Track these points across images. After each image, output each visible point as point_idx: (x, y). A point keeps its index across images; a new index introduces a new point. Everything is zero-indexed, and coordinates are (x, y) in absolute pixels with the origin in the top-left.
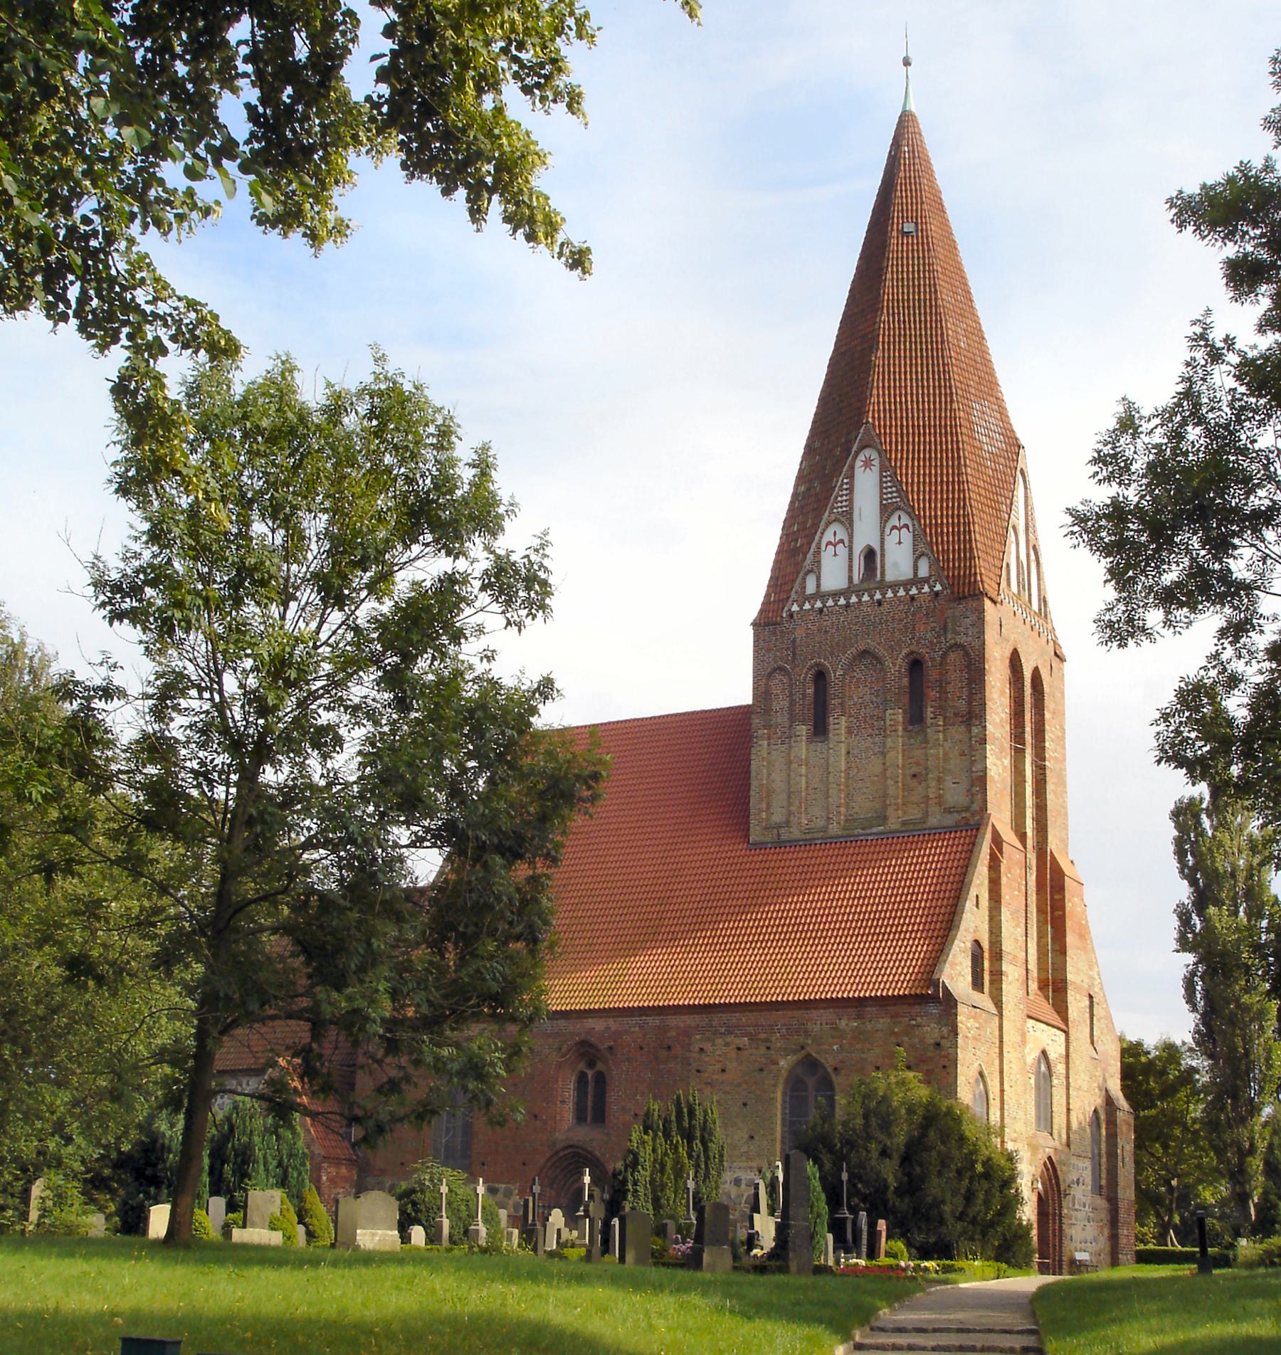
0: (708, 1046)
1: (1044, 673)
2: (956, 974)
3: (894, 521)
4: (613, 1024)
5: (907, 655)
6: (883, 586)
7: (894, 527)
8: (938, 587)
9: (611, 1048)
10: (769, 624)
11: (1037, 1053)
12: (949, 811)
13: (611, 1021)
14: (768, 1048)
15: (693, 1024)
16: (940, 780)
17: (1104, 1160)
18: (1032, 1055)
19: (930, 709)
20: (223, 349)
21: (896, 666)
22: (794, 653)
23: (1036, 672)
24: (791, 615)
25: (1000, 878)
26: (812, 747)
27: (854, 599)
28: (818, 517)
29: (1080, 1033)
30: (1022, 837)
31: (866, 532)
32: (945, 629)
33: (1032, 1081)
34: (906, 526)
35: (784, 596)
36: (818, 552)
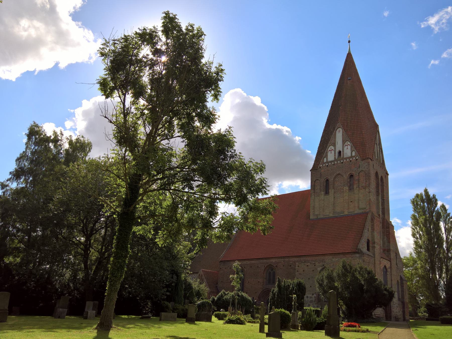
1: (384, 177)
3: (346, 144)
4: (277, 260)
6: (343, 159)
8: (357, 158)
12: (360, 209)
16: (358, 202)
17: (400, 292)
18: (382, 267)
20: (147, 37)
21: (346, 177)
23: (382, 177)
27: (336, 162)
29: (394, 262)
31: (339, 146)
36: (327, 153)
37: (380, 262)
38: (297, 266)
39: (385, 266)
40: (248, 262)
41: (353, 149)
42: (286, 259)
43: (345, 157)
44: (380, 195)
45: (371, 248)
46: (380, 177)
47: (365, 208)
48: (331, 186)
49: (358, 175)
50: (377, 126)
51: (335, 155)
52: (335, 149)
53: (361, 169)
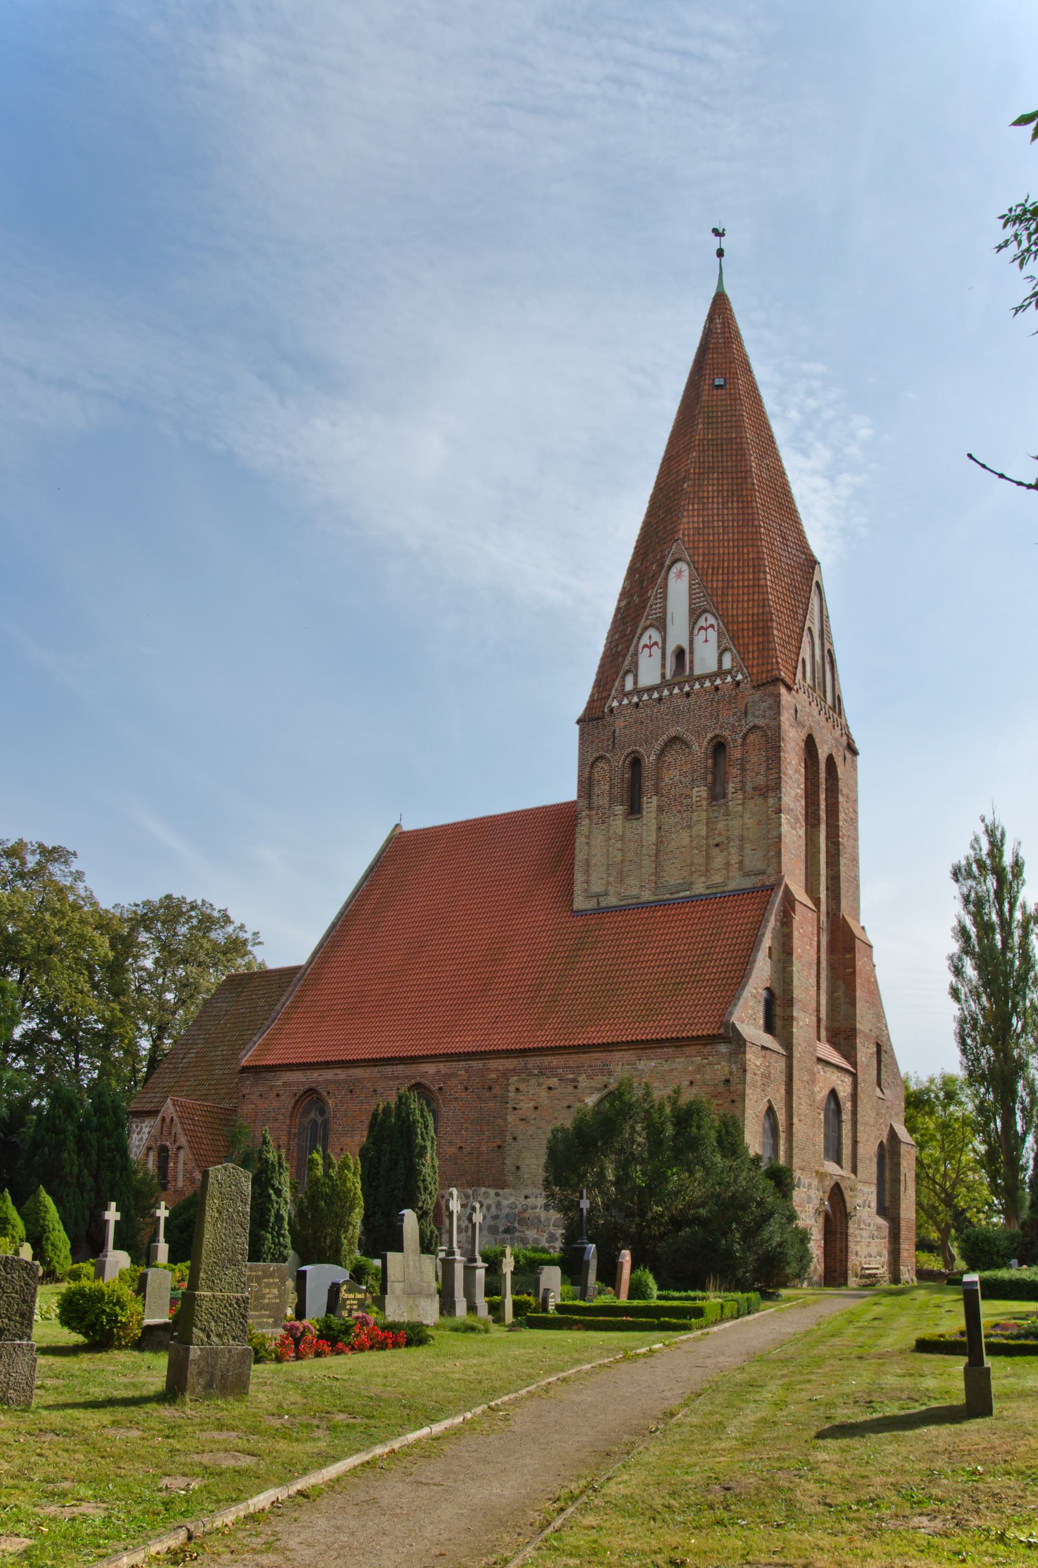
0: (522, 1086)
1: (838, 760)
2: (748, 1018)
3: (702, 622)
4: (443, 1067)
5: (712, 739)
6: (692, 679)
7: (702, 628)
8: (740, 677)
9: (440, 1089)
10: (592, 720)
11: (826, 1092)
12: (747, 875)
13: (441, 1065)
14: (576, 1087)
15: (511, 1067)
16: (741, 848)
18: (822, 1093)
19: (731, 785)
21: (700, 747)
22: (614, 743)
23: (830, 759)
24: (611, 711)
25: (791, 932)
26: (628, 824)
28: (635, 626)
30: (817, 902)
31: (678, 634)
32: (746, 713)
33: (822, 1117)
34: (712, 626)
35: (605, 694)
36: (636, 654)
37: (813, 1074)
38: (512, 1088)
39: (833, 1093)
40: (342, 1074)
41: (727, 642)
42: (474, 1064)
43: (697, 672)
44: (823, 827)
45: (778, 1023)
46: (822, 757)
47: (763, 873)
48: (648, 785)
49: (743, 745)
50: (812, 563)
51: (663, 666)
52: (664, 640)
53: (751, 721)
